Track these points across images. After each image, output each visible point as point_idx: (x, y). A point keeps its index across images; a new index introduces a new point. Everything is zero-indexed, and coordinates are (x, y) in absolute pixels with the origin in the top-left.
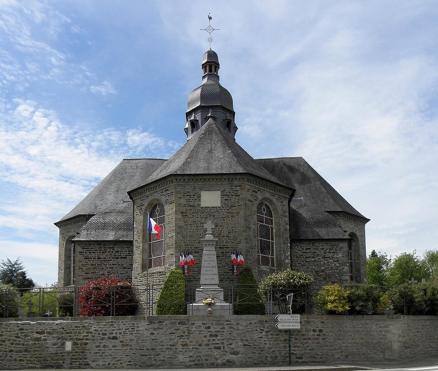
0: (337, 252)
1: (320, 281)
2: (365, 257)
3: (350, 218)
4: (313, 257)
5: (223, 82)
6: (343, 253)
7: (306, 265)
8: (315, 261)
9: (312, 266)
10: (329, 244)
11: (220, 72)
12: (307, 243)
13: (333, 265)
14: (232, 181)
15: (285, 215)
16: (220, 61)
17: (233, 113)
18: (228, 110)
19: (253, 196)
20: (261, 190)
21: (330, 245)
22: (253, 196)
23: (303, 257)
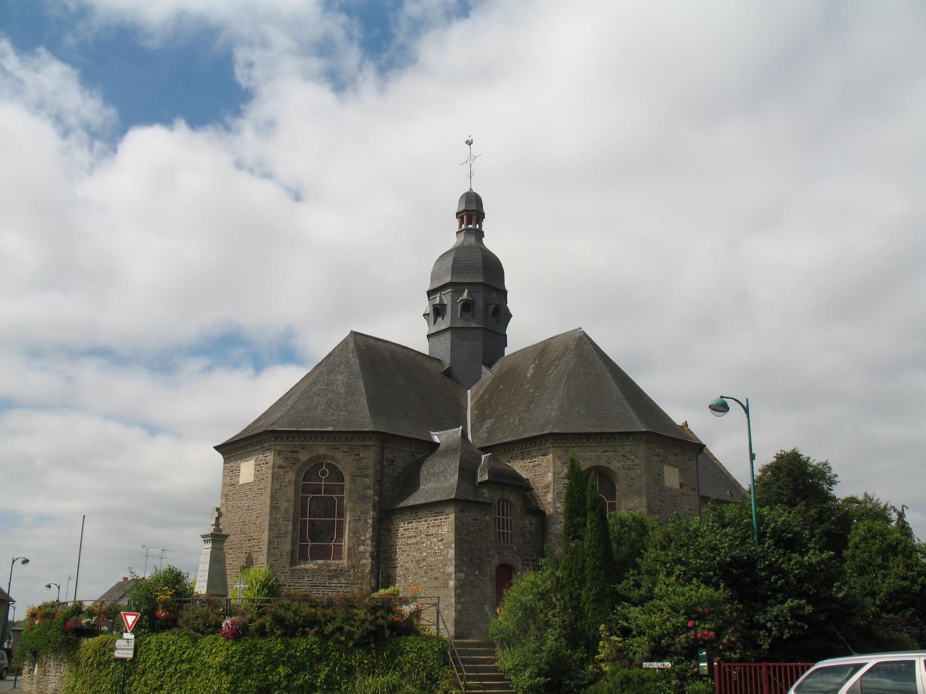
0: (441, 525)
1: (421, 577)
2: (858, 531)
3: (659, 442)
4: (415, 537)
5: (490, 242)
6: (449, 525)
7: (406, 551)
8: (417, 543)
9: (413, 552)
10: (433, 512)
11: (486, 226)
12: (409, 513)
13: (437, 548)
14: (262, 444)
15: (364, 473)
16: (486, 208)
17: (504, 293)
18: (496, 289)
19: (289, 459)
20: (308, 446)
21: (435, 513)
22: (289, 459)
23: (404, 538)
